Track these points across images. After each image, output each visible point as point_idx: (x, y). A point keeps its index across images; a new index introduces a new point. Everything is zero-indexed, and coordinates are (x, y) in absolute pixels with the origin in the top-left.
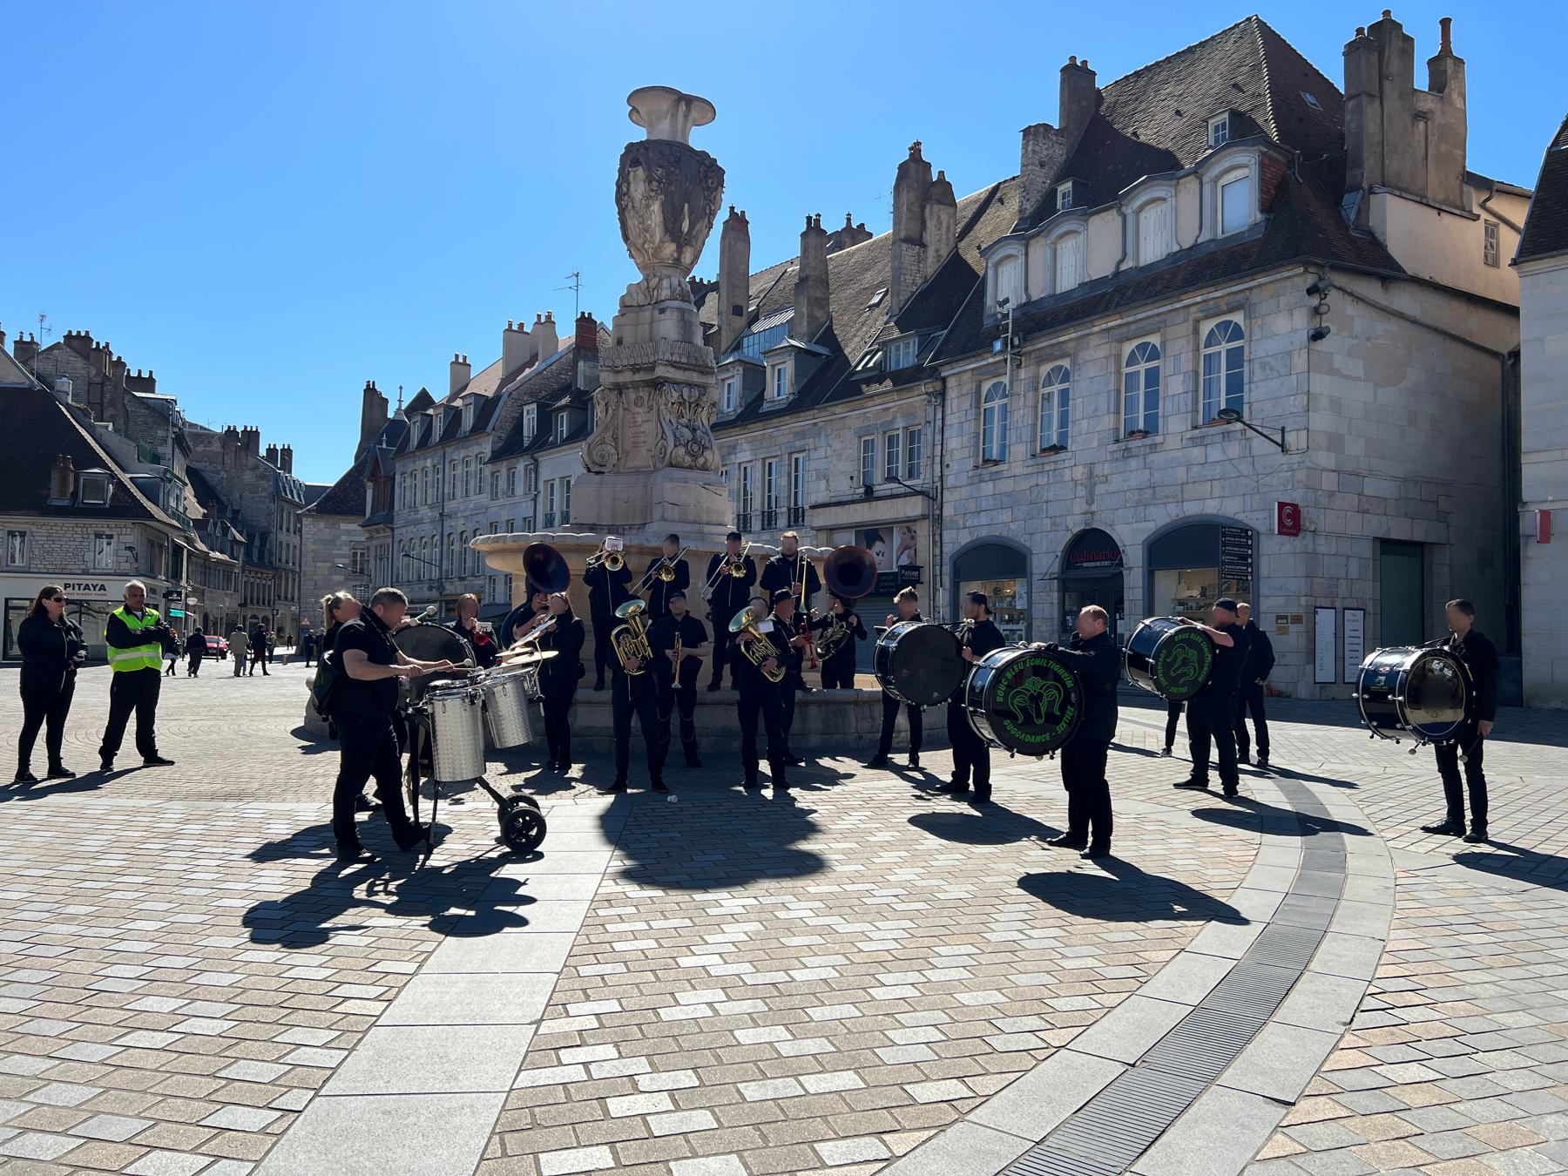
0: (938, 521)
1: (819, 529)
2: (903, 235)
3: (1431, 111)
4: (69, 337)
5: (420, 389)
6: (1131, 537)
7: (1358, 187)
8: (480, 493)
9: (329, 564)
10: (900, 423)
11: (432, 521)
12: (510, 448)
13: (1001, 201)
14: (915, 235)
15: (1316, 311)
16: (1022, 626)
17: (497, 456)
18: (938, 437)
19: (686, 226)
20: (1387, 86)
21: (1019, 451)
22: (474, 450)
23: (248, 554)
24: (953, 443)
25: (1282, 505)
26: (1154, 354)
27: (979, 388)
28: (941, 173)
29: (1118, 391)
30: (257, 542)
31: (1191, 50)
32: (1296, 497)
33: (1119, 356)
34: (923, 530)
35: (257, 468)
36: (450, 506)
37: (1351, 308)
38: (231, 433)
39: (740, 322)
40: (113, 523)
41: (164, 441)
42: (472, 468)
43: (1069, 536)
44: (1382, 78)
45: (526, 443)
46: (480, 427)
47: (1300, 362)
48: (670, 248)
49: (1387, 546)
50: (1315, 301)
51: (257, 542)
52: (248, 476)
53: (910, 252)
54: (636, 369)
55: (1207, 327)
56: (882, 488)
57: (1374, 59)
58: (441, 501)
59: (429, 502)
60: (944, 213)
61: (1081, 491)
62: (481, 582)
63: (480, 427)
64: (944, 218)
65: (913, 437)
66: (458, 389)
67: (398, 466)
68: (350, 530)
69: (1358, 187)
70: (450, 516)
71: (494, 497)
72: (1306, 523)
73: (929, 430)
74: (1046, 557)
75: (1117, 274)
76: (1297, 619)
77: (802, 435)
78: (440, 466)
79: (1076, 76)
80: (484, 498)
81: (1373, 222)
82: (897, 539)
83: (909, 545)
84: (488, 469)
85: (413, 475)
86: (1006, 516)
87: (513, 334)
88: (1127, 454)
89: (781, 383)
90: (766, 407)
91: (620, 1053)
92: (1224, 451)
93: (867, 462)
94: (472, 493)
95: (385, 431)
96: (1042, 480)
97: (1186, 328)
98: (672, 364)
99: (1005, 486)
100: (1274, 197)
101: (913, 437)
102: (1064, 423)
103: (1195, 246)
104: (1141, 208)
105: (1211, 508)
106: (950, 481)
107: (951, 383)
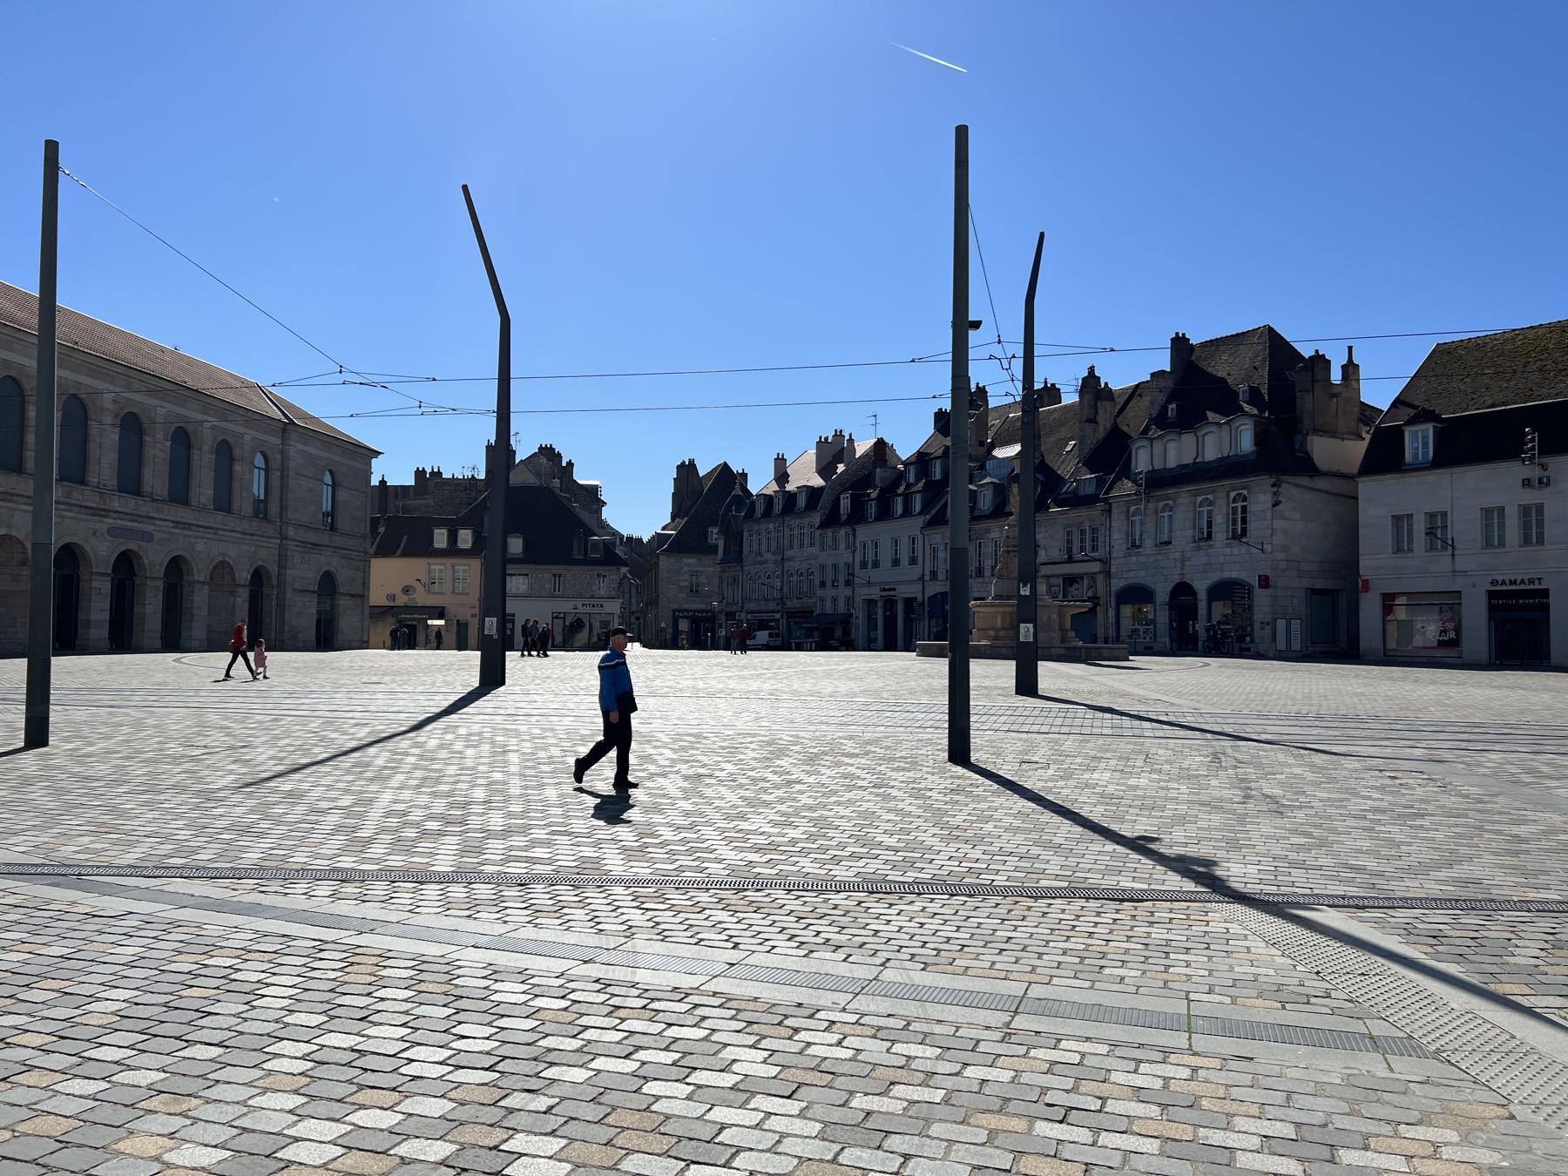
0: (1108, 574)
3: (1340, 393)
4: (541, 448)
6: (1201, 586)
7: (1301, 432)
11: (775, 562)
12: (831, 520)
13: (1140, 396)
15: (1275, 494)
16: (1152, 627)
17: (824, 525)
18: (1108, 533)
21: (1149, 543)
22: (806, 521)
24: (1116, 536)
25: (1259, 576)
26: (1211, 503)
27: (1128, 510)
28: (1106, 384)
29: (1195, 519)
32: (1267, 572)
33: (1195, 503)
34: (1100, 579)
36: (789, 553)
37: (1293, 490)
39: (982, 450)
40: (606, 568)
43: (1173, 585)
45: (844, 518)
47: (1269, 514)
49: (1314, 592)
50: (1275, 489)
53: (1089, 427)
55: (1233, 494)
56: (1077, 556)
57: (1310, 374)
60: (1108, 405)
61: (1178, 564)
62: (812, 600)
64: (1108, 408)
66: (782, 477)
69: (1301, 432)
70: (789, 559)
71: (822, 549)
72: (1271, 583)
73: (1103, 528)
74: (1162, 595)
75: (1195, 463)
76: (1268, 624)
81: (1308, 448)
82: (1086, 582)
83: (1093, 585)
84: (818, 533)
86: (1143, 573)
88: (1199, 548)
92: (1238, 550)
93: (1069, 542)
96: (1160, 557)
101: (1094, 530)
103: (1228, 456)
104: (1206, 434)
105: (1234, 575)
107: (1114, 506)
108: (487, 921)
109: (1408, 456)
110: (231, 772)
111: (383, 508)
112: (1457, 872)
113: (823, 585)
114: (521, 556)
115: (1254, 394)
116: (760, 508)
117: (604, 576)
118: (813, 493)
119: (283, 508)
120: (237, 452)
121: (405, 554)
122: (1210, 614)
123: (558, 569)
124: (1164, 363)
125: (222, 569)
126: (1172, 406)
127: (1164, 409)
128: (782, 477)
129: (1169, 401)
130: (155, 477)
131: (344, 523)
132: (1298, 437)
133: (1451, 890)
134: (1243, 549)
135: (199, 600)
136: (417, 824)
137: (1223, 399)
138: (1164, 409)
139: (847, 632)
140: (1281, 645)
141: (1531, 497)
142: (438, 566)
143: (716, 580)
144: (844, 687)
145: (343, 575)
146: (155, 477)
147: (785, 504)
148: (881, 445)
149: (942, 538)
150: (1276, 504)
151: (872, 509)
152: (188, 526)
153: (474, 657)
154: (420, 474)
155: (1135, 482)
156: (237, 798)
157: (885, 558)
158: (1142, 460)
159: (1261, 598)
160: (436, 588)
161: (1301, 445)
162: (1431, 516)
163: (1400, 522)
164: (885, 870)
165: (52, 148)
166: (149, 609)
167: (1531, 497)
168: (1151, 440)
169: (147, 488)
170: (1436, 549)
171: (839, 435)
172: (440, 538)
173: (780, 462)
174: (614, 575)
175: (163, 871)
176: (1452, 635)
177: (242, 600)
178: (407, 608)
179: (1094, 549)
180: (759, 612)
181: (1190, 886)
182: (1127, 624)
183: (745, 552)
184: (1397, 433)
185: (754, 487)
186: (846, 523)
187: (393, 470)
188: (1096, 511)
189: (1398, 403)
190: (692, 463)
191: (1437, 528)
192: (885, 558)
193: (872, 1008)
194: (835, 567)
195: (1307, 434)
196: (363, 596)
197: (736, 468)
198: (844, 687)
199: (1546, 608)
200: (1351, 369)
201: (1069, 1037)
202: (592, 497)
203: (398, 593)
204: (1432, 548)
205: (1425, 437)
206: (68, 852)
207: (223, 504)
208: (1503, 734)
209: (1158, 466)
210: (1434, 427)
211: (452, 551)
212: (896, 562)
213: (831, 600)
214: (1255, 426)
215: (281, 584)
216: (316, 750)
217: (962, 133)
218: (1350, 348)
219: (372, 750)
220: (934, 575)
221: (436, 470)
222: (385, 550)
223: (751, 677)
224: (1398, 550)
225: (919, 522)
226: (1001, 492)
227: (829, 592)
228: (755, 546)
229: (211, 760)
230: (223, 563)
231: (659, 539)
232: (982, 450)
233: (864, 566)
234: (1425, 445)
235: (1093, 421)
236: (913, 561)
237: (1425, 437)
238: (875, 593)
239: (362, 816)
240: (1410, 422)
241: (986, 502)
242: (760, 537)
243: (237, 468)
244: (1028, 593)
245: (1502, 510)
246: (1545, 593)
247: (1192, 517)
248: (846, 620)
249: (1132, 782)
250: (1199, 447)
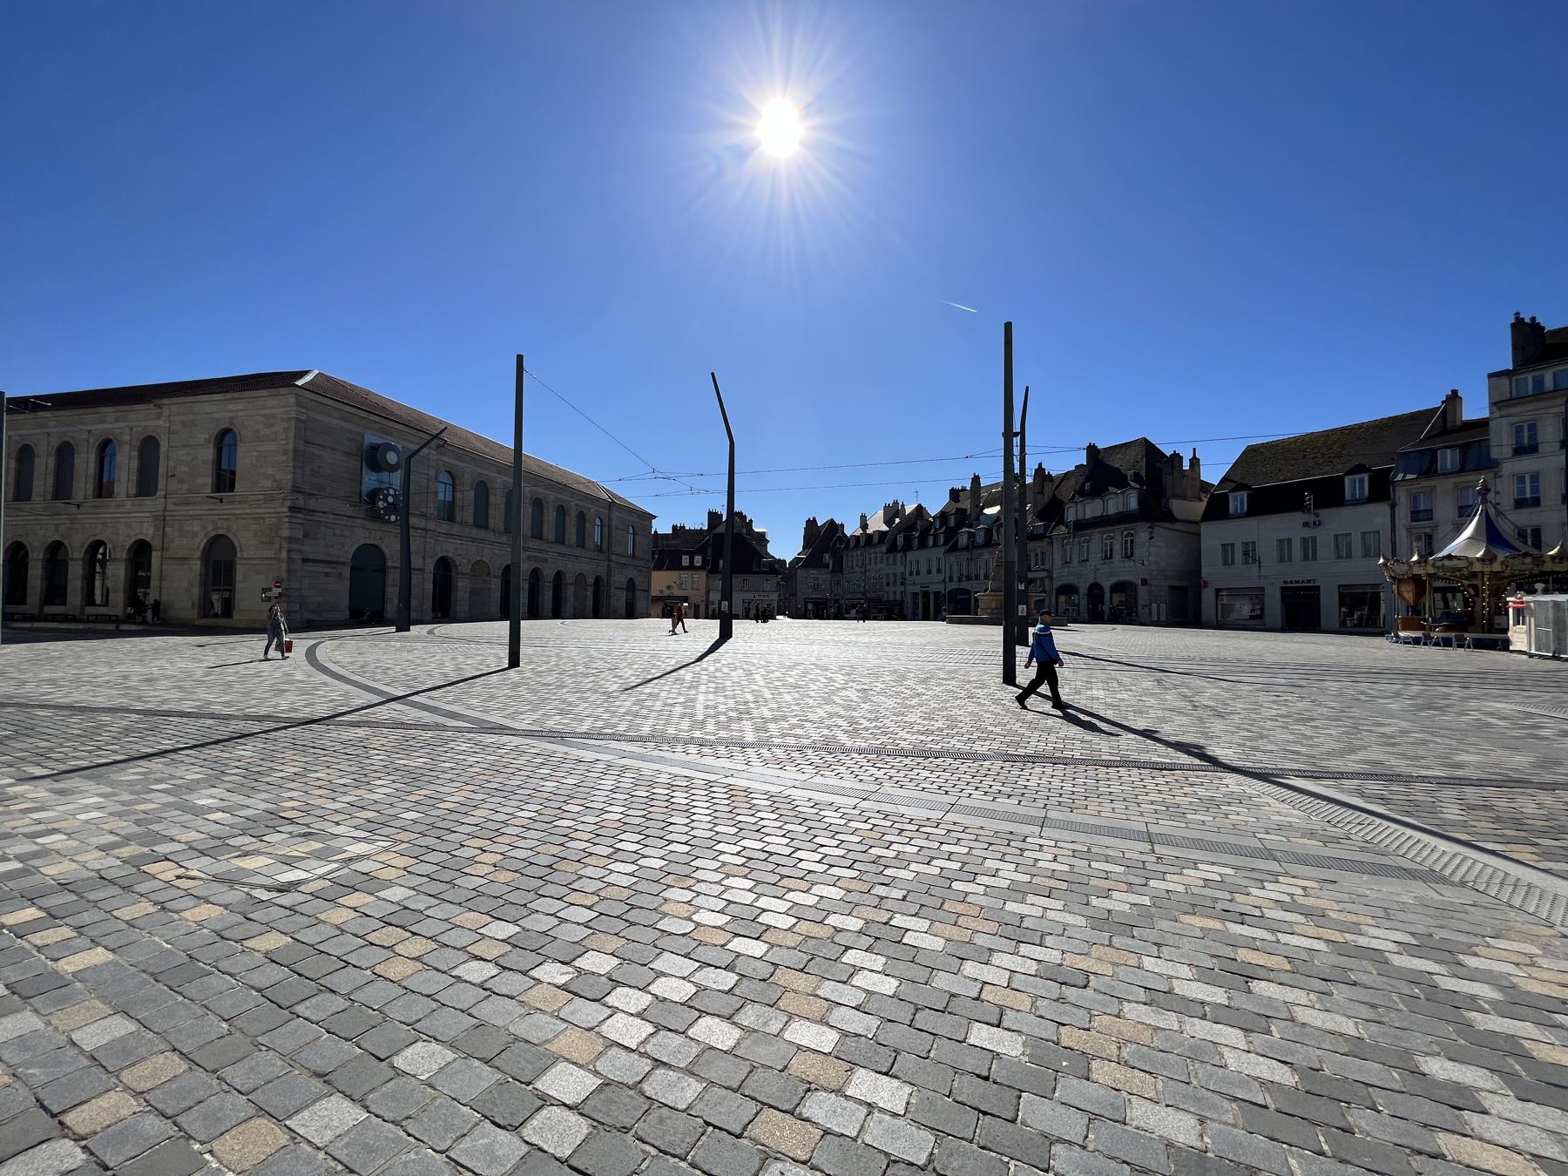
6: (1106, 585)
12: (893, 549)
17: (888, 551)
21: (1075, 561)
24: (1055, 556)
26: (1112, 538)
34: (1047, 580)
36: (869, 567)
37: (1161, 530)
49: (1172, 588)
66: (864, 526)
74: (1083, 590)
79: (1091, 449)
91: (642, 1093)
100: (1142, 501)
101: (1043, 554)
102: (1088, 554)
105: (1126, 578)
108: (791, 771)
109: (1231, 510)
110: (616, 683)
111: (656, 545)
112: (1361, 755)
113: (888, 585)
115: (1137, 477)
116: (852, 544)
118: (882, 534)
119: (609, 545)
120: (587, 518)
121: (668, 569)
122: (1110, 601)
123: (746, 576)
124: (1082, 459)
125: (581, 578)
127: (1083, 485)
128: (864, 526)
129: (1086, 481)
130: (549, 531)
131: (639, 554)
132: (1164, 500)
133: (1357, 768)
134: (1132, 563)
135: (570, 592)
136: (725, 714)
137: (1119, 480)
138: (1083, 485)
139: (901, 610)
140: (1155, 618)
141: (1308, 533)
142: (684, 575)
143: (828, 582)
144: (917, 641)
145: (638, 581)
146: (549, 531)
147: (867, 541)
148: (920, 509)
150: (1151, 539)
151: (916, 543)
152: (564, 555)
153: (716, 623)
154: (674, 527)
155: (1067, 527)
156: (623, 697)
157: (923, 570)
158: (1071, 515)
159: (1142, 591)
160: (684, 586)
162: (1246, 544)
163: (1227, 549)
164: (959, 745)
165: (520, 358)
166: (546, 598)
167: (1308, 533)
168: (1076, 503)
169: (545, 536)
170: (1284, 561)
171: (896, 503)
172: (685, 561)
173: (863, 518)
174: (775, 580)
175: (599, 736)
176: (1258, 612)
177: (590, 592)
178: (669, 597)
181: (1197, 762)
182: (1062, 607)
184: (1225, 496)
185: (848, 532)
186: (900, 551)
187: (662, 526)
189: (1224, 480)
190: (814, 519)
191: (1250, 552)
192: (923, 570)
193: (1063, 838)
194: (895, 575)
196: (648, 591)
197: (838, 522)
198: (917, 641)
199: (1317, 597)
201: (1203, 862)
202: (762, 538)
203: (665, 589)
204: (1247, 562)
205: (1242, 499)
206: (550, 724)
207: (581, 544)
208: (1354, 674)
209: (1080, 518)
210: (1248, 494)
211: (692, 567)
212: (929, 572)
213: (892, 593)
214: (1139, 495)
215: (608, 585)
216: (653, 671)
217: (1008, 327)
218: (1194, 449)
219: (682, 672)
220: (951, 579)
222: (658, 567)
223: (862, 634)
224: (1226, 563)
225: (943, 549)
226: (988, 532)
227: (891, 589)
228: (850, 564)
229: (603, 676)
230: (581, 574)
231: (796, 560)
233: (911, 574)
234: (1242, 503)
235: (1041, 493)
236: (939, 571)
237: (1242, 499)
238: (917, 589)
239: (693, 707)
240: (1233, 490)
241: (980, 538)
242: (851, 560)
243: (588, 525)
245: (1289, 541)
246: (1318, 588)
248: (901, 604)
249: (1119, 696)
250: (1105, 508)
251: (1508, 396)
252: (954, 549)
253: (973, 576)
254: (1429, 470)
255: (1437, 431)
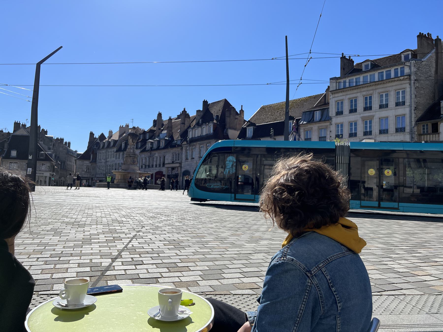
0: (181, 167)
1: (166, 167)
2: (182, 123)
3: (238, 118)
5: (102, 133)
8: (114, 157)
9: (81, 170)
10: (177, 152)
11: (104, 163)
14: (183, 122)
17: (117, 151)
19: (134, 141)
20: (231, 115)
22: (113, 150)
23: (61, 167)
30: (63, 164)
31: (219, 101)
35: (63, 147)
36: (108, 160)
38: (57, 139)
39: (160, 131)
40: (45, 162)
41: (51, 145)
42: (112, 153)
44: (230, 114)
45: (122, 149)
46: (114, 146)
48: (132, 143)
51: (63, 164)
52: (61, 149)
53: (183, 125)
54: (128, 155)
58: (106, 159)
59: (104, 158)
60: (188, 119)
63: (114, 146)
65: (179, 154)
66: (110, 136)
67: (98, 152)
68: (87, 163)
69: (226, 128)
70: (108, 162)
71: (116, 159)
75: (201, 136)
77: (165, 153)
78: (106, 152)
79: (205, 103)
80: (114, 159)
82: (176, 169)
84: (115, 154)
85: (101, 153)
86: (188, 167)
87: (121, 128)
89: (162, 144)
90: (160, 148)
94: (112, 157)
95: (95, 144)
96: (192, 162)
97: (205, 145)
98: (132, 155)
99: (188, 163)
101: (179, 154)
106: (183, 161)
107: (183, 147)
109: (247, 136)
114: (16, 157)
117: (45, 164)
126: (201, 120)
149: (144, 156)
161: (226, 132)
179: (178, 160)
180: (100, 178)
183: (97, 159)
188: (179, 149)
195: (228, 129)
200: (241, 111)
209: (193, 137)
210: (253, 128)
221: (111, 131)
232: (160, 131)
234: (251, 132)
244: (31, 158)
247: (199, 151)
251: (335, 89)
252: (144, 151)
253: (151, 165)
254: (311, 121)
255: (322, 104)
